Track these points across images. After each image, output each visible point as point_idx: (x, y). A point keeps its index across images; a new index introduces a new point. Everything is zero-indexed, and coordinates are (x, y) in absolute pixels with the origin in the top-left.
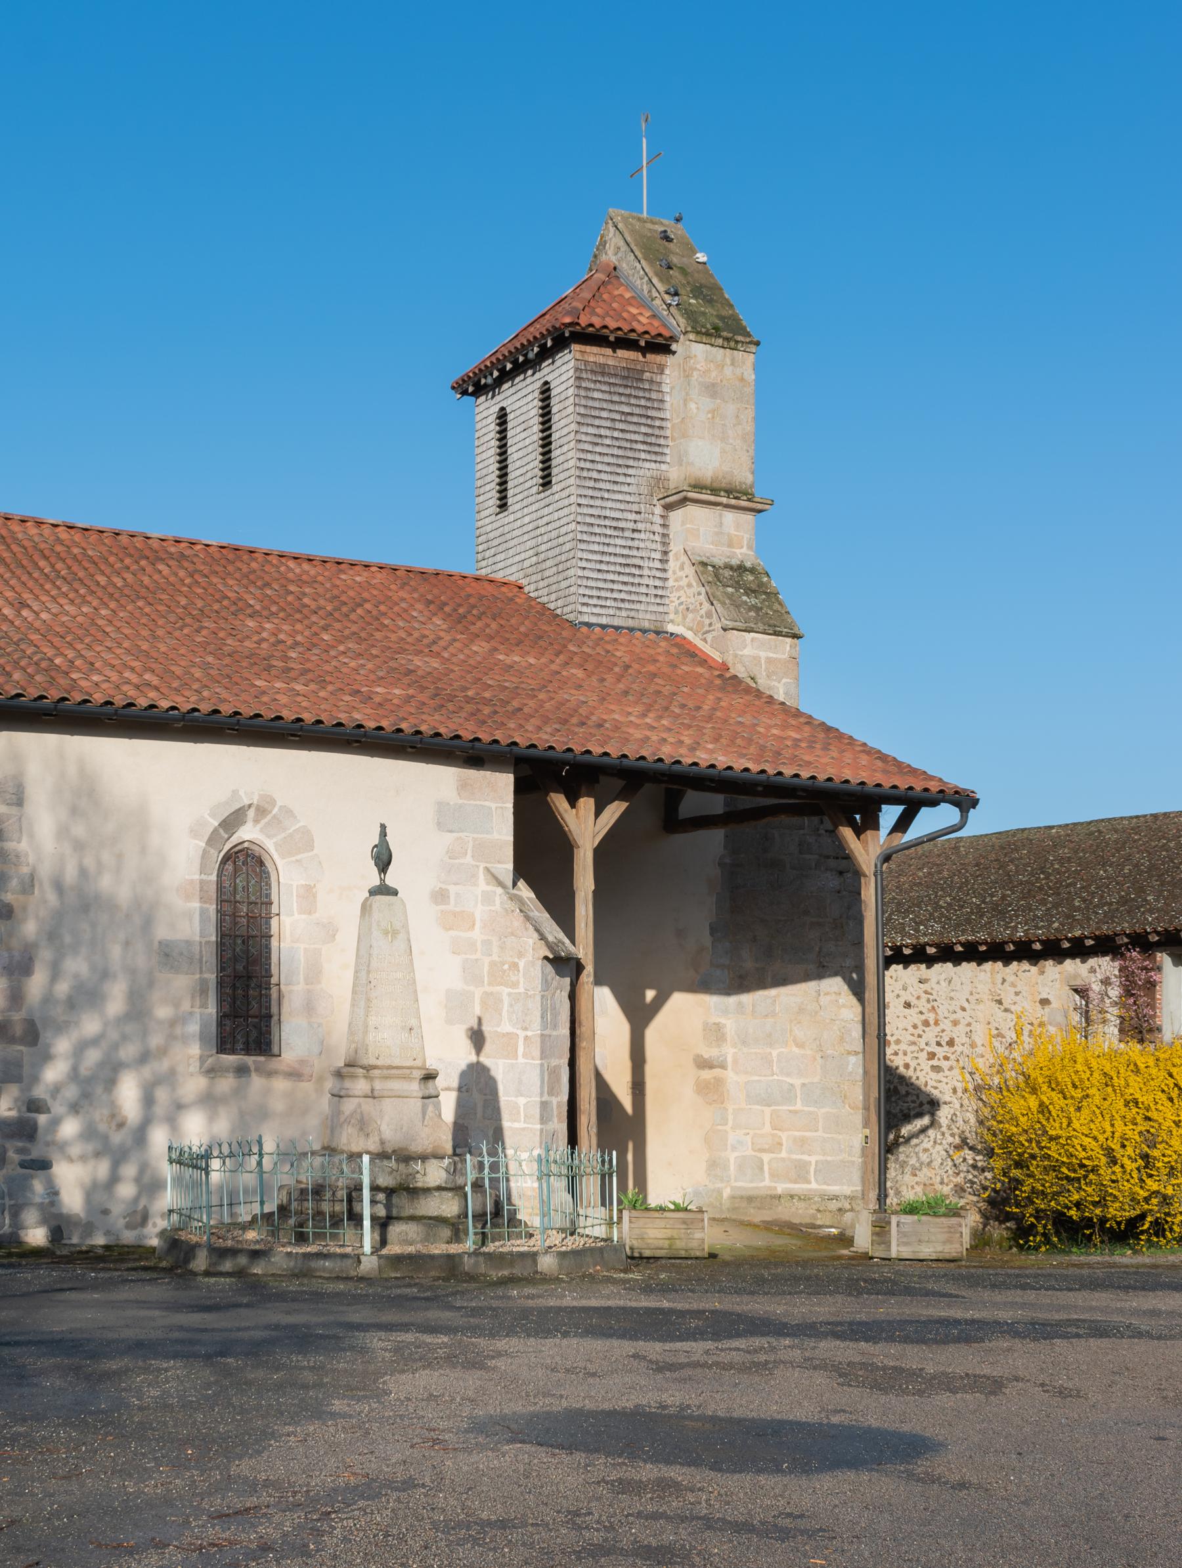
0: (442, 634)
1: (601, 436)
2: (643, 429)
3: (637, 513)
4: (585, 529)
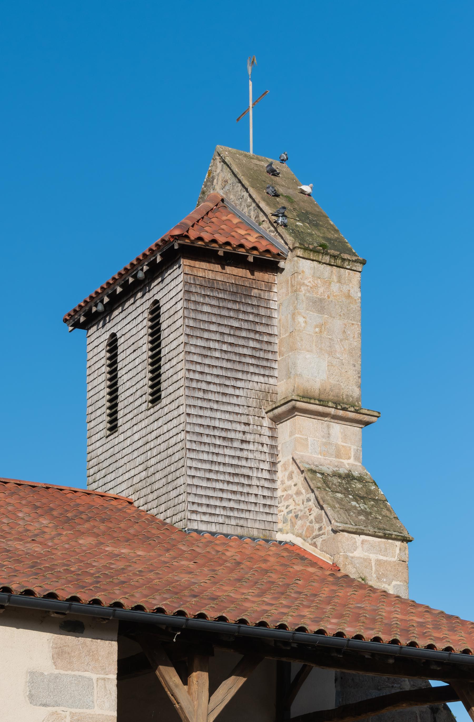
0: (46, 530)
1: (210, 349)
2: (252, 344)
3: (245, 424)
4: (195, 438)
